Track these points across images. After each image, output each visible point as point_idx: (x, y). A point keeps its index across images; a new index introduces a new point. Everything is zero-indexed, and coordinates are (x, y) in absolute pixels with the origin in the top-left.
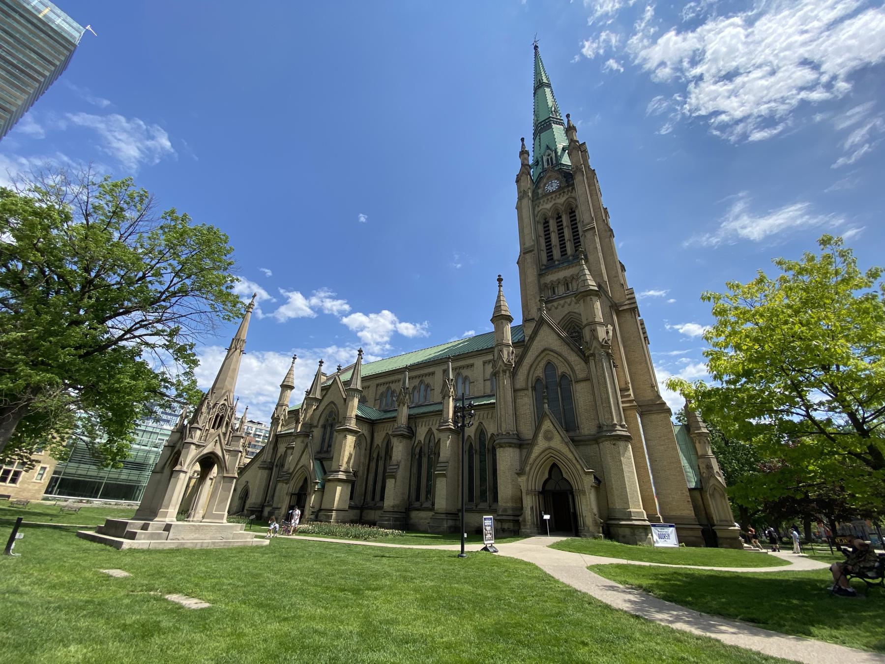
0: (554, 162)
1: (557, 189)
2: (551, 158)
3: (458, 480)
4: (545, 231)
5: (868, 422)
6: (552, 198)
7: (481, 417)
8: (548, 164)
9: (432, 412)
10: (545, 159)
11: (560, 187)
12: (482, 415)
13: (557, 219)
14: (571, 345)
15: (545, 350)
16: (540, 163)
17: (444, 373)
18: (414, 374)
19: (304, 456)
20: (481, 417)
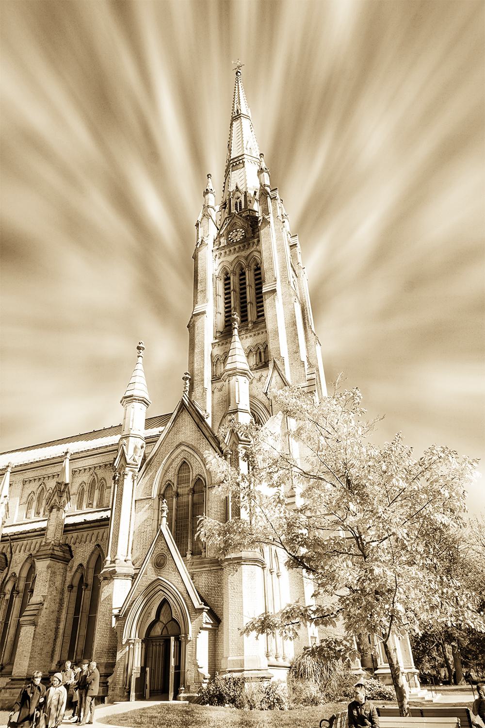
0: (243, 207)
1: (241, 240)
2: (240, 203)
3: (57, 629)
4: (256, 280)
5: (360, 533)
6: (254, 243)
7: (100, 538)
8: (236, 209)
9: (35, 531)
10: (233, 202)
11: (245, 237)
12: (101, 534)
13: (256, 270)
14: (210, 439)
15: (180, 444)
16: (228, 206)
17: (10, 486)
18: (80, 464)
19: (183, 587)
20: (100, 538)
